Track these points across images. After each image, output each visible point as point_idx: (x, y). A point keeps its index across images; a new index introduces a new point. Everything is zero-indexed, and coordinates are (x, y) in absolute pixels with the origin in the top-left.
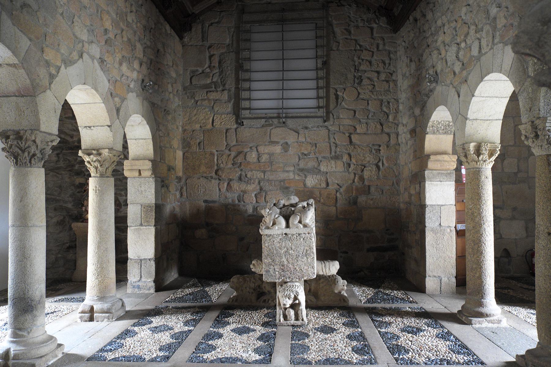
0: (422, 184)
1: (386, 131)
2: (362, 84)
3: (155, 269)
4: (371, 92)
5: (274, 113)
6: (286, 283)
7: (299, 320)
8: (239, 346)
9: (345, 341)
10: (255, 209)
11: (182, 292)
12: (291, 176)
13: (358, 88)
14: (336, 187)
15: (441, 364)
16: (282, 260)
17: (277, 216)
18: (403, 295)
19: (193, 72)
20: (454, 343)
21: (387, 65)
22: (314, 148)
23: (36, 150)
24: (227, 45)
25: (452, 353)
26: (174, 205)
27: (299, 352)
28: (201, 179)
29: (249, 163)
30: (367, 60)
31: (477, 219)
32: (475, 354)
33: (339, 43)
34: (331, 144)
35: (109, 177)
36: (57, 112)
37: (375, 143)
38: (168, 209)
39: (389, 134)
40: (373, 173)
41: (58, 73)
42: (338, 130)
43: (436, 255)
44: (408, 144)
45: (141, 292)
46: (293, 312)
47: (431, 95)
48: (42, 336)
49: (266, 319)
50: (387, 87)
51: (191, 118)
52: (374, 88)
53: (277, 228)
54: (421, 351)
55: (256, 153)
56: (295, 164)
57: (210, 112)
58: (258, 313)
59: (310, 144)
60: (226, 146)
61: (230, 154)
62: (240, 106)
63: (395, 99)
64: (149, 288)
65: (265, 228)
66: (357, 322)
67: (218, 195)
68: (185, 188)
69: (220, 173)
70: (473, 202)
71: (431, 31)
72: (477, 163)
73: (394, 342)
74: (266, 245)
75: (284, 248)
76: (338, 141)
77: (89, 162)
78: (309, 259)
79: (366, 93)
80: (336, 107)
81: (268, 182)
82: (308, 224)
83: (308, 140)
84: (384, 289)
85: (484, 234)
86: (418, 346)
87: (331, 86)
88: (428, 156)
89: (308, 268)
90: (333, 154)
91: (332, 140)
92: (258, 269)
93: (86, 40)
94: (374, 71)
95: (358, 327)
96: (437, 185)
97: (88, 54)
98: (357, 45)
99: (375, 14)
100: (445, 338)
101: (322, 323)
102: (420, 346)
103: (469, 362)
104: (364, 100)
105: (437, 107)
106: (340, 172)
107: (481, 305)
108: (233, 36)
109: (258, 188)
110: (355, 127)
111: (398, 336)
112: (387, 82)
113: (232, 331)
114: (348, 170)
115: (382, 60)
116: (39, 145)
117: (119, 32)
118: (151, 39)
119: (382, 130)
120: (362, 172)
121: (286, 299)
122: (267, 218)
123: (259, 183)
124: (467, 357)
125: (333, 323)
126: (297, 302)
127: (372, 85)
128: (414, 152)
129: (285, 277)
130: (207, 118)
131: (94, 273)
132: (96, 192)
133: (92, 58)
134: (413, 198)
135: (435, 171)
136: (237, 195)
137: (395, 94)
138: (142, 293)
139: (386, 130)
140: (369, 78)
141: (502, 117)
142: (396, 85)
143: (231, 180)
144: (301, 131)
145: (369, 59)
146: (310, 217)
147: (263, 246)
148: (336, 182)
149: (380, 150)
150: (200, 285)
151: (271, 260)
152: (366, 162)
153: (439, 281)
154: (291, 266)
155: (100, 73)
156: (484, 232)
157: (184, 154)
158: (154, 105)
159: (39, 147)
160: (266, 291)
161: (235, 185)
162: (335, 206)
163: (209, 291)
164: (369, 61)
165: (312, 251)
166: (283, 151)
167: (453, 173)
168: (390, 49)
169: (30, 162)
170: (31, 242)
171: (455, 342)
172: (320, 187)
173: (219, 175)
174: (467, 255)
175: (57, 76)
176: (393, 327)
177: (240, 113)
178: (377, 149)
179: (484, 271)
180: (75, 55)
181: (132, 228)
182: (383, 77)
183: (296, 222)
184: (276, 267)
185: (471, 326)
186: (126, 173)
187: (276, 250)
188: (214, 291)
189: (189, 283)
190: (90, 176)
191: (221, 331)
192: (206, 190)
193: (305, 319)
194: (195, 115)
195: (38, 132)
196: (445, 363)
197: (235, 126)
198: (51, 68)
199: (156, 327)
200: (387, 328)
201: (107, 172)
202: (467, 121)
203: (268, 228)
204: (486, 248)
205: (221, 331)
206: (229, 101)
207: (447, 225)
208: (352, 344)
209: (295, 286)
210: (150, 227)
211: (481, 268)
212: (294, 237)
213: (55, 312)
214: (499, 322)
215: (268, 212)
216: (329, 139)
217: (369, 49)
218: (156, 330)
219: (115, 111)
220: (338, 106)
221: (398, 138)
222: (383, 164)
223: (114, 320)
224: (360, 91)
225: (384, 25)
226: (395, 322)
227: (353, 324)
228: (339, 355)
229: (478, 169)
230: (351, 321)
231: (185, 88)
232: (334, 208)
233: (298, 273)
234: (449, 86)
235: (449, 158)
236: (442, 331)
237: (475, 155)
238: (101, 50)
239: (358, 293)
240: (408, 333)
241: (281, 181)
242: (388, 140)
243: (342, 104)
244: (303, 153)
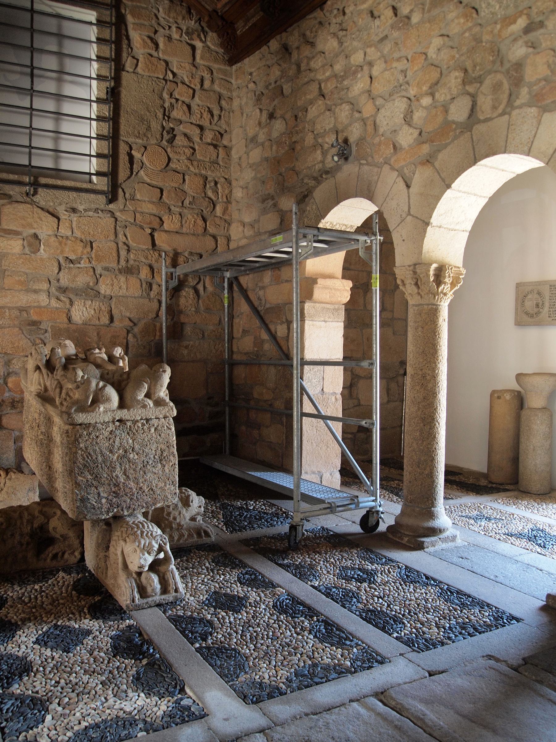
2: (174, 143)
7: (169, 592)
12: (43, 299)
13: (169, 150)
14: (127, 323)
21: (216, 118)
22: (89, 249)
30: (183, 102)
31: (430, 385)
33: (138, 60)
34: (120, 246)
37: (193, 251)
39: (214, 237)
40: (190, 302)
42: (133, 221)
43: (316, 439)
50: (214, 156)
52: (193, 154)
53: (102, 409)
59: (82, 241)
63: (226, 179)
65: (75, 410)
70: (425, 358)
72: (435, 297)
75: (119, 449)
76: (132, 240)
78: (166, 468)
79: (181, 161)
83: (78, 234)
87: (122, 138)
89: (165, 486)
90: (123, 263)
91: (121, 236)
94: (195, 125)
98: (169, 72)
99: (200, 23)
104: (178, 173)
105: (345, 200)
106: (135, 297)
107: (431, 515)
110: (161, 219)
112: (215, 146)
114: (148, 295)
115: (209, 108)
121: (144, 555)
129: (119, 509)
137: (226, 170)
139: (211, 230)
140: (185, 135)
141: (469, 228)
142: (228, 155)
144: (64, 214)
145: (187, 100)
148: (128, 314)
151: (92, 475)
154: (132, 484)
156: (438, 405)
160: (58, 536)
164: (187, 105)
165: (171, 451)
168: (222, 91)
172: (97, 322)
182: (209, 137)
183: (141, 396)
187: (102, 455)
202: (429, 228)
212: (138, 427)
214: (454, 538)
215: (83, 377)
216: (116, 235)
217: (188, 84)
220: (133, 175)
222: (205, 287)
224: (171, 156)
225: (213, 47)
229: (435, 307)
233: (145, 497)
241: (21, 310)
243: (139, 174)
244: (67, 258)
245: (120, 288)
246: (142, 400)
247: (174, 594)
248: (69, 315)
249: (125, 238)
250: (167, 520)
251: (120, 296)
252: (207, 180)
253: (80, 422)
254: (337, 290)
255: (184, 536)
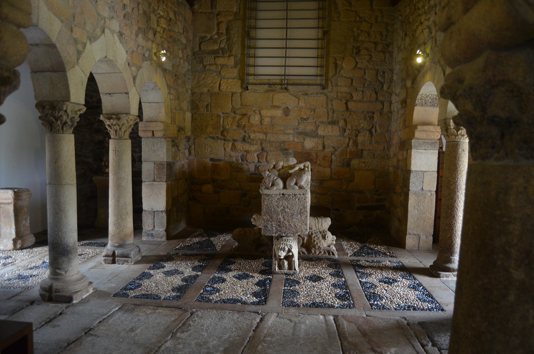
0: (409, 151)
1: (380, 99)
3: (167, 220)
4: (368, 62)
5: (277, 80)
6: (282, 237)
8: (240, 290)
9: (330, 289)
10: (257, 168)
11: (190, 241)
12: (291, 138)
13: (357, 58)
15: (408, 310)
16: (279, 217)
17: (275, 178)
18: (385, 250)
19: (202, 38)
20: (422, 292)
21: (384, 37)
22: (313, 113)
23: (67, 118)
24: (235, 12)
25: (419, 301)
26: (183, 162)
27: (290, 297)
28: (208, 139)
29: (252, 126)
31: (452, 187)
32: (437, 302)
35: (126, 139)
36: (83, 84)
38: (178, 166)
40: (366, 138)
41: (84, 49)
44: (399, 113)
45: (154, 240)
46: (287, 262)
47: (421, 70)
48: (76, 275)
49: (263, 268)
51: (200, 82)
52: (371, 58)
53: (275, 189)
54: (393, 299)
55: (259, 116)
56: (294, 128)
57: (217, 77)
58: (256, 262)
59: (310, 109)
60: (232, 109)
61: (235, 117)
62: (246, 72)
64: (162, 236)
65: (264, 188)
66: (342, 272)
67: (223, 154)
68: (193, 147)
69: (225, 133)
71: (425, 10)
73: (372, 291)
74: (265, 203)
75: (281, 207)
77: (109, 126)
80: (335, 75)
81: (270, 144)
82: (303, 187)
84: (370, 244)
85: (457, 200)
86: (392, 294)
88: (415, 127)
89: (302, 225)
91: (330, 105)
92: (258, 222)
93: (107, 17)
95: (342, 277)
96: (422, 153)
97: (109, 28)
100: (415, 289)
101: (311, 272)
102: (393, 295)
103: (431, 308)
108: (240, 5)
109: (260, 148)
110: (351, 95)
111: (375, 286)
112: (384, 53)
113: (234, 277)
114: (343, 135)
115: (380, 32)
116: (69, 114)
117: (136, 5)
118: (164, 9)
119: (377, 98)
120: (356, 137)
121: (281, 251)
122: (267, 180)
123: (261, 144)
124: (431, 305)
125: (321, 273)
126: (291, 254)
127: (369, 55)
128: (404, 121)
130: (214, 82)
131: (115, 223)
132: (116, 153)
133: (113, 32)
134: (400, 163)
135: (421, 140)
136: (240, 155)
138: (155, 241)
139: (381, 98)
142: (391, 56)
143: (235, 141)
146: (307, 179)
147: (262, 205)
148: (332, 145)
149: (373, 117)
150: (206, 235)
151: (269, 216)
152: (360, 128)
153: (418, 239)
154: (286, 222)
155: (118, 44)
156: (457, 199)
157: (192, 115)
158: (166, 71)
159: (70, 116)
161: (240, 145)
162: (330, 167)
163: (214, 241)
166: (284, 115)
167: (437, 143)
169: (62, 129)
170: (65, 198)
171: (423, 292)
173: (224, 136)
174: (441, 217)
175: (83, 52)
176: (372, 278)
177: (245, 78)
178: (371, 116)
179: (454, 232)
180: (98, 31)
181: (146, 183)
182: (380, 47)
183: (293, 184)
184: (273, 223)
185: (439, 278)
186: (141, 134)
188: (219, 241)
189: (196, 233)
190: (110, 138)
191: (224, 276)
192: (212, 149)
193: (297, 268)
194: (203, 79)
195: (68, 103)
196: (412, 309)
197: (240, 91)
198: (79, 45)
199: (168, 271)
200: (367, 279)
201: (125, 134)
203: (267, 188)
204: (458, 212)
205: (224, 276)
206: (236, 67)
207: (428, 190)
208: (336, 291)
209: (289, 240)
210: (161, 183)
211: (452, 229)
212: (290, 198)
213: (83, 254)
215: (268, 174)
216: (327, 105)
218: (168, 273)
219: (132, 79)
221: (391, 106)
222: (376, 130)
223: (133, 263)
224: (358, 61)
226: (375, 273)
227: (337, 275)
228: (323, 300)
229: (456, 143)
230: (337, 271)
231: (194, 54)
232: (329, 169)
234: (436, 64)
235: (434, 129)
236: (414, 282)
237: (454, 130)
238: (120, 25)
239: (345, 247)
240: (385, 283)
242: (382, 107)
245: (328, 131)
246: (293, 186)
247: (293, 271)
248: (303, 145)
249: (331, 106)
250: (314, 244)
251: (328, 136)
252: (378, 71)
253: (266, 193)
254: (431, 132)
255: (321, 253)
